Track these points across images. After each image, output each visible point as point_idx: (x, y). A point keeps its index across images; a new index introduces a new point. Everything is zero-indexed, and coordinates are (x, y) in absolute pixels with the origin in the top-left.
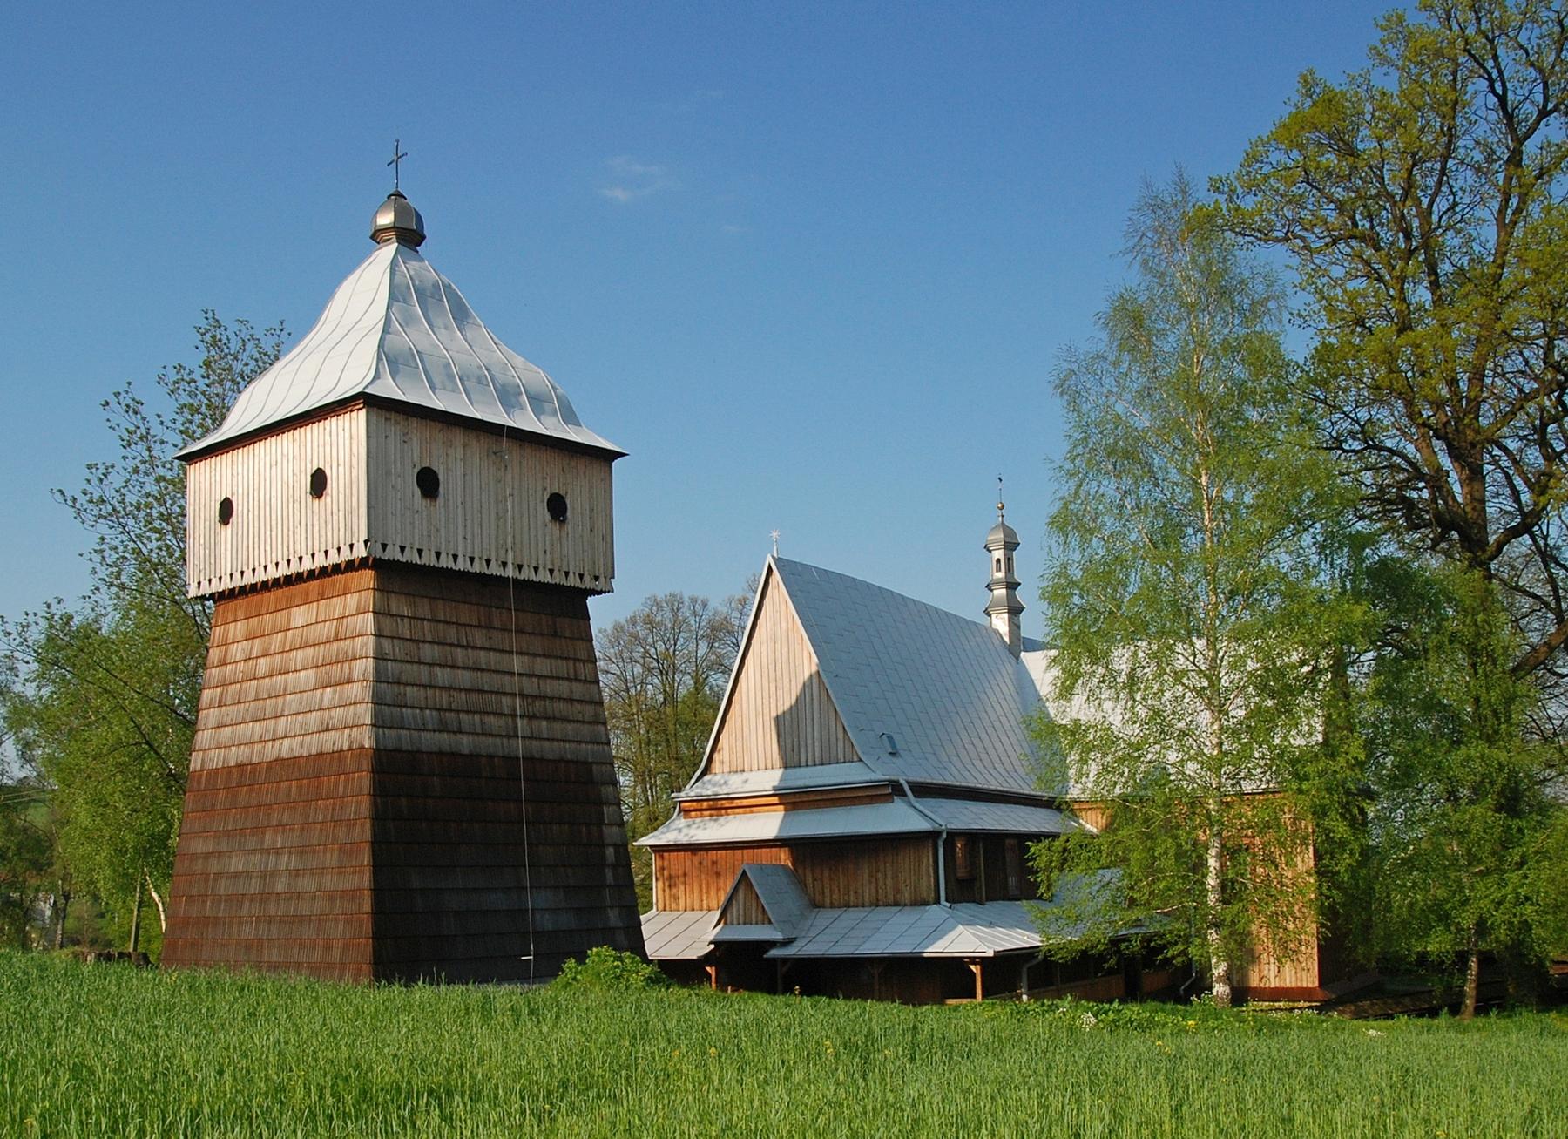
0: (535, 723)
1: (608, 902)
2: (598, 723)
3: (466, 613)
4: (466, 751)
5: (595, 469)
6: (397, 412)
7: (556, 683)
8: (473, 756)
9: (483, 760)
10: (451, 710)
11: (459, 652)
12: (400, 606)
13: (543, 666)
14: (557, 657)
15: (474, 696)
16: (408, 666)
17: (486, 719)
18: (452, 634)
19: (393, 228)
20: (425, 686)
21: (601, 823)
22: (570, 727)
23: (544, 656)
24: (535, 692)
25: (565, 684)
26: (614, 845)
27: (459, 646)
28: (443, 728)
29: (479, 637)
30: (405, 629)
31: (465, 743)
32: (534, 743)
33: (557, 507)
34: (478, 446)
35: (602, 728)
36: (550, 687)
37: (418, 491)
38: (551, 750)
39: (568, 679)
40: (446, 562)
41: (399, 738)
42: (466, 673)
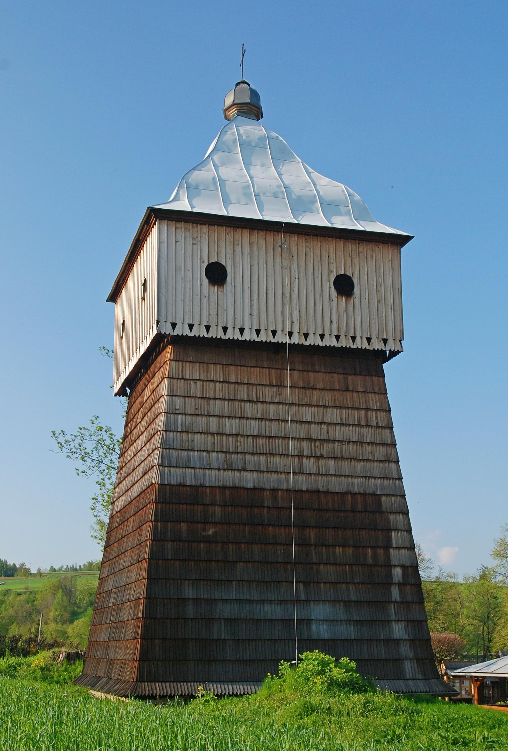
0: (322, 462)
1: (393, 617)
2: (389, 462)
3: (257, 375)
4: (250, 485)
5: (383, 253)
6: (186, 221)
7: (346, 429)
8: (256, 490)
9: (267, 493)
10: (237, 453)
11: (249, 407)
12: (193, 371)
13: (334, 415)
14: (347, 408)
15: (260, 441)
16: (198, 418)
17: (271, 459)
18: (242, 393)
19: (234, 104)
20: (212, 434)
21: (388, 546)
22: (358, 465)
23: (335, 407)
24: (324, 436)
25: (355, 430)
26: (403, 567)
27: (249, 401)
28: (229, 467)
29: (269, 394)
30: (196, 389)
31: (249, 480)
32: (320, 478)
33: (344, 286)
34: (261, 240)
35: (393, 466)
36: (339, 433)
37: (206, 281)
38: (337, 485)
39: (359, 425)
40: (233, 334)
41: (184, 475)
42: (255, 423)
